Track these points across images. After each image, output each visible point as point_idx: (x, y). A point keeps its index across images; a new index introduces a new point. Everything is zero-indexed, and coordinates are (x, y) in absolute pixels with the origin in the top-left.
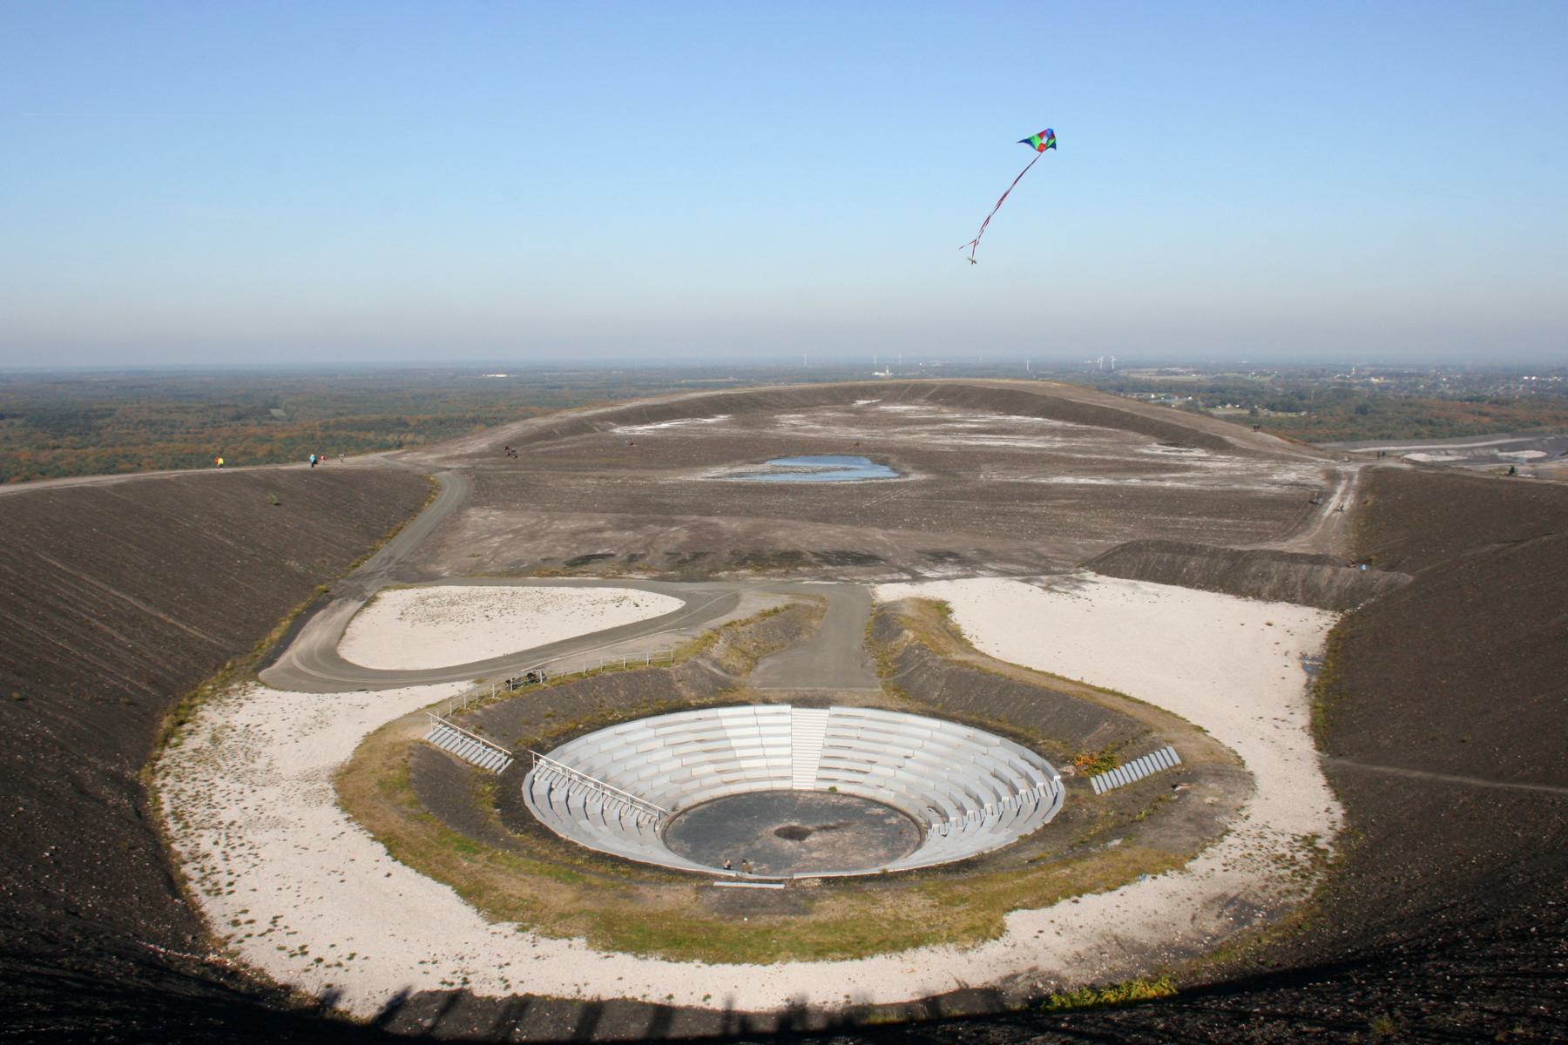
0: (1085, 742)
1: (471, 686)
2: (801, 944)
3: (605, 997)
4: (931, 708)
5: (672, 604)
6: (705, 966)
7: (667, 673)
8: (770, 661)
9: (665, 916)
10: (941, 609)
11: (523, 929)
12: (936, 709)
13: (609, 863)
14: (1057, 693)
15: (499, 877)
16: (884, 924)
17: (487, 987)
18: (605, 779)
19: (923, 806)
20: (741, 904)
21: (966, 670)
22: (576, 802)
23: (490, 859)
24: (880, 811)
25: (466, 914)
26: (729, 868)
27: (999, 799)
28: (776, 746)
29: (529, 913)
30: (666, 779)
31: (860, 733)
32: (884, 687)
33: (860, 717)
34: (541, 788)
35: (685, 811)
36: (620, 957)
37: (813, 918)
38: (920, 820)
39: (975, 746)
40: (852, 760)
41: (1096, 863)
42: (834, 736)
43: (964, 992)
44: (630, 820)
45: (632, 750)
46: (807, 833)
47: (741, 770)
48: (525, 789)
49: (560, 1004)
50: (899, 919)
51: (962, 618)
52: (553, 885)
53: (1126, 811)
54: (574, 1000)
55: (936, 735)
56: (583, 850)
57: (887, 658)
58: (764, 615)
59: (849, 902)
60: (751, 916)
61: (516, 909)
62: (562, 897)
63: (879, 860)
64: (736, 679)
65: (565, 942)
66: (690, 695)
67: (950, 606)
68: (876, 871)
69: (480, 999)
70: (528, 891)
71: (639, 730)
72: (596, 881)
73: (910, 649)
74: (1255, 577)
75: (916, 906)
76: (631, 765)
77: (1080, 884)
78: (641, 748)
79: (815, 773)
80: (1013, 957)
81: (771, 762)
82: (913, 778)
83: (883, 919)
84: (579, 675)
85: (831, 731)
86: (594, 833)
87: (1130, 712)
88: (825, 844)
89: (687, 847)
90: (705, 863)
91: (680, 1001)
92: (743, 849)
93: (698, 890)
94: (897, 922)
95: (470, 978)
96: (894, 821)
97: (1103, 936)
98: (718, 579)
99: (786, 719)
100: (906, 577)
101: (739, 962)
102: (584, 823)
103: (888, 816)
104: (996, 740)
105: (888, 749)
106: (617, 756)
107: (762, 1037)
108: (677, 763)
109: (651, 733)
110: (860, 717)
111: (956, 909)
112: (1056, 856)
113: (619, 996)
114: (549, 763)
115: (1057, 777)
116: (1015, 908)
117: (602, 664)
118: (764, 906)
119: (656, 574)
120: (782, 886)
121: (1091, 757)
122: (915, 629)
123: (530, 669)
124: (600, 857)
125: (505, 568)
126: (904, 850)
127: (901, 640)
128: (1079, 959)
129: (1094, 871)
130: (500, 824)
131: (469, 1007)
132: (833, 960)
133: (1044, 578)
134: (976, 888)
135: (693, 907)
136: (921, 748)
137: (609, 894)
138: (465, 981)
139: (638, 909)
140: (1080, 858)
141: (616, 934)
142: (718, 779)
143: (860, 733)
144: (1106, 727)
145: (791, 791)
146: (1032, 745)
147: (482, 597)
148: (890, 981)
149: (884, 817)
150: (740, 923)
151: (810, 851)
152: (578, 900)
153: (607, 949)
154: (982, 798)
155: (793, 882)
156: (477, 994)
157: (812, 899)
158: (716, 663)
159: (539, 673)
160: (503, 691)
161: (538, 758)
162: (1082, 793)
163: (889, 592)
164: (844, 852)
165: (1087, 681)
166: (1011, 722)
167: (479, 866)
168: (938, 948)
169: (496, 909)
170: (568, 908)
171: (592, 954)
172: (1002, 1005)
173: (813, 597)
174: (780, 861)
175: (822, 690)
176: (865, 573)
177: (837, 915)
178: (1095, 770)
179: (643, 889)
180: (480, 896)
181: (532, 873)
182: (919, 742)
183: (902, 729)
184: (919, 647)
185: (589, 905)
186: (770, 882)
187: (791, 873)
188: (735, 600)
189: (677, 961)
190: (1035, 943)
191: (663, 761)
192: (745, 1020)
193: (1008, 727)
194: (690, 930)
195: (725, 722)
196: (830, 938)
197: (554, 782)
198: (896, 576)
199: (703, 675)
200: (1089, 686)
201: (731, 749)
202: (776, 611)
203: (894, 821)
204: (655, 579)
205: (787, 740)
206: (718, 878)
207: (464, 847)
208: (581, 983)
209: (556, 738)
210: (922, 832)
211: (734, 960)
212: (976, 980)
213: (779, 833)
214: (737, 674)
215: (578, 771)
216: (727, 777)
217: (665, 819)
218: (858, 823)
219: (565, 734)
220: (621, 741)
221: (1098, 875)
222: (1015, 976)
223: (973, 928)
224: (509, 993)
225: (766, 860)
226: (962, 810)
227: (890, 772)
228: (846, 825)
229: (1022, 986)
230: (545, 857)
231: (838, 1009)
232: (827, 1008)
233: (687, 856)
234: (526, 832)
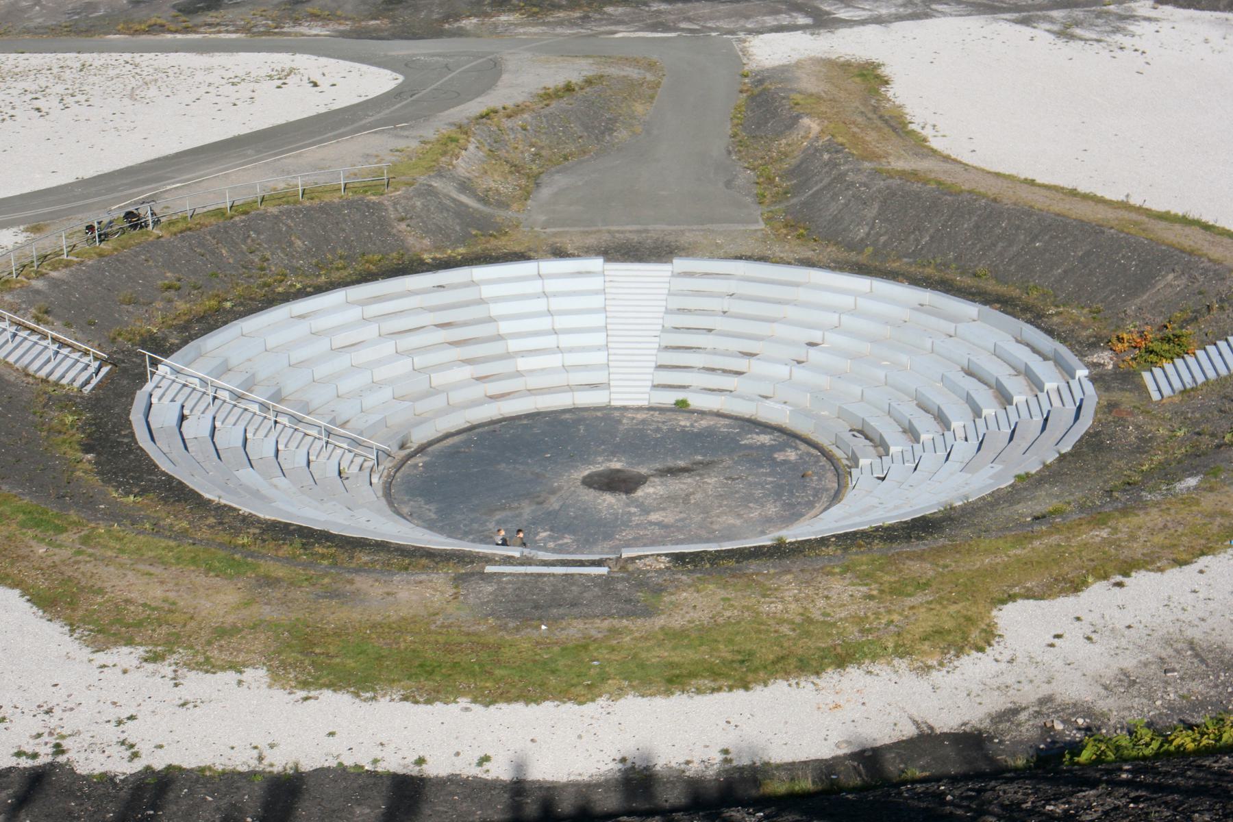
0: (1131, 309)
1: (21, 238)
2: (642, 666)
3: (307, 766)
4: (853, 256)
5: (377, 81)
6: (477, 708)
7: (378, 206)
8: (561, 181)
9: (402, 627)
10: (870, 77)
11: (154, 658)
12: (862, 259)
13: (298, 541)
14: (1082, 224)
15: (103, 570)
16: (785, 629)
17: (97, 757)
18: (278, 397)
19: (843, 429)
20: (533, 602)
21: (916, 187)
22: (229, 437)
23: (85, 540)
24: (765, 439)
25: (50, 637)
26: (505, 543)
27: (977, 412)
28: (578, 330)
29: (164, 630)
30: (386, 393)
31: (726, 304)
32: (768, 220)
33: (727, 276)
34: (164, 415)
35: (422, 449)
36: (327, 696)
37: (660, 621)
38: (838, 453)
39: (933, 321)
40: (715, 352)
41: (1154, 517)
42: (681, 311)
43: (926, 740)
44: (326, 466)
45: (323, 345)
46: (640, 481)
47: (519, 374)
48: (136, 417)
49: (231, 780)
50: (810, 621)
51: (909, 93)
52: (201, 580)
53: (1207, 427)
54: (254, 773)
55: (863, 303)
56: (248, 521)
57: (772, 169)
58: (548, 96)
59: (722, 593)
60: (553, 621)
61: (140, 624)
62: (219, 600)
63: (768, 521)
64: (501, 215)
65: (231, 676)
66: (420, 245)
67: (885, 71)
68: (765, 541)
69: (87, 778)
70: (159, 592)
71: (334, 309)
72: (280, 571)
73: (812, 153)
75: (840, 597)
76: (321, 371)
77: (1125, 554)
78: (340, 340)
79: (650, 376)
80: (1010, 679)
81: (571, 359)
82: (823, 381)
83: (781, 622)
84: (219, 213)
85: (677, 303)
86: (265, 489)
87: (1216, 253)
88: (672, 498)
89: (431, 511)
90: (464, 535)
91: (437, 768)
92: (527, 510)
93: (459, 580)
94: (806, 625)
95: (66, 744)
96: (792, 455)
97: (1168, 642)
98: (461, 33)
99: (596, 283)
100: (802, 20)
101: (537, 700)
102: (246, 475)
103: (781, 448)
104: (970, 309)
105: (779, 330)
106: (298, 355)
107: (1058, 819)
108: (404, 366)
109: (355, 313)
110: (727, 276)
111: (909, 601)
112: (1082, 508)
113: (333, 763)
114: (177, 372)
115: (1082, 373)
116: (1012, 598)
117: (260, 194)
118: (573, 605)
119: (346, 26)
120: (603, 570)
121: (1142, 335)
122: (821, 116)
123: (128, 205)
124: (280, 532)
125: (63, 20)
126: (810, 505)
127: (795, 136)
128: (1127, 681)
129: (1152, 532)
130: (96, 480)
131: (70, 793)
132: (699, 691)
133: (1056, 14)
134: (941, 564)
135: (451, 609)
136: (836, 328)
137: (295, 591)
138: (59, 750)
139: (356, 616)
140: (1125, 511)
141: (319, 660)
143: (726, 304)
144: (1170, 282)
145: (608, 409)
146: (1036, 317)
147: (24, 75)
148: (799, 724)
149: (773, 449)
150: (535, 634)
151: (646, 511)
152: (247, 604)
153: (305, 685)
154: (949, 412)
155: (624, 564)
156: (82, 770)
157: (659, 590)
158: (465, 186)
159: (144, 211)
160: (82, 246)
161: (155, 363)
162: (1127, 399)
163: (773, 49)
164: (706, 510)
165: (1136, 201)
166: (1000, 278)
167: (66, 553)
168: (879, 667)
169: (105, 627)
170: (231, 619)
171: (280, 695)
172: (991, 760)
173: (634, 62)
174: (593, 529)
175: (658, 230)
176: (729, 16)
177: (702, 616)
178: (1151, 357)
179: (363, 582)
180: (73, 605)
181: (160, 561)
182: (833, 318)
183: (802, 294)
184: (828, 148)
185: (268, 612)
186: (581, 564)
187: (617, 549)
188: (491, 72)
189: (429, 702)
190: (1048, 656)
191: (380, 362)
192: (549, 793)
193: (992, 286)
194: (448, 648)
195: (487, 291)
196: (691, 655)
197: (192, 406)
198: (785, 19)
199: (442, 208)
200: (1139, 210)
201: (500, 337)
202: (569, 88)
203: (792, 455)
204: (343, 35)
205: (598, 320)
206: (489, 560)
207: (36, 521)
208: (263, 744)
209: (185, 327)
210: (842, 473)
211: (530, 696)
212: (947, 720)
213: (589, 482)
214: (503, 205)
215: (230, 383)
217: (387, 464)
218: (728, 462)
219: (201, 319)
220: (302, 328)
221: (1159, 539)
222: (1015, 711)
223: (939, 632)
224: (137, 766)
225: (568, 528)
226: (912, 433)
227: (782, 371)
228: (707, 465)
229: (1027, 728)
230: (184, 534)
231: (711, 773)
232: (692, 771)
233: (431, 526)
234: (143, 492)
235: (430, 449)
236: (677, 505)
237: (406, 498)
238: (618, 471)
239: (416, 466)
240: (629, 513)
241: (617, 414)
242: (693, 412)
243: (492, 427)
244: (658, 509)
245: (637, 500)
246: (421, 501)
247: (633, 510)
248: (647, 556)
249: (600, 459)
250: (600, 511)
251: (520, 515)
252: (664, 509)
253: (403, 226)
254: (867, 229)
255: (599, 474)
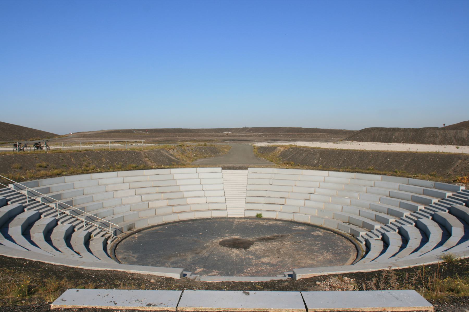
31: (271, 182)
35: (139, 231)
74: (430, 137)
92: (190, 257)
142: (170, 210)
143: (271, 182)
145: (227, 218)
151: (259, 257)
175: (244, 165)
195: (176, 177)
213: (223, 244)
216: (175, 209)
227: (302, 203)
235: (143, 231)
236: (274, 254)
237: (123, 251)
238: (237, 239)
239: (135, 237)
240: (249, 258)
241: (231, 220)
242: (265, 219)
243: (175, 224)
244: (264, 256)
245: (251, 252)
246: (131, 252)
247: (251, 257)
248: (329, 276)
249: (227, 235)
250: (232, 257)
251: (186, 259)
252: (268, 256)
253: (147, 159)
254: (317, 161)
255: (228, 241)
